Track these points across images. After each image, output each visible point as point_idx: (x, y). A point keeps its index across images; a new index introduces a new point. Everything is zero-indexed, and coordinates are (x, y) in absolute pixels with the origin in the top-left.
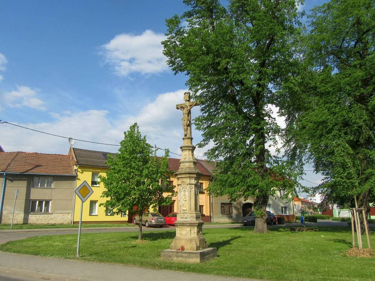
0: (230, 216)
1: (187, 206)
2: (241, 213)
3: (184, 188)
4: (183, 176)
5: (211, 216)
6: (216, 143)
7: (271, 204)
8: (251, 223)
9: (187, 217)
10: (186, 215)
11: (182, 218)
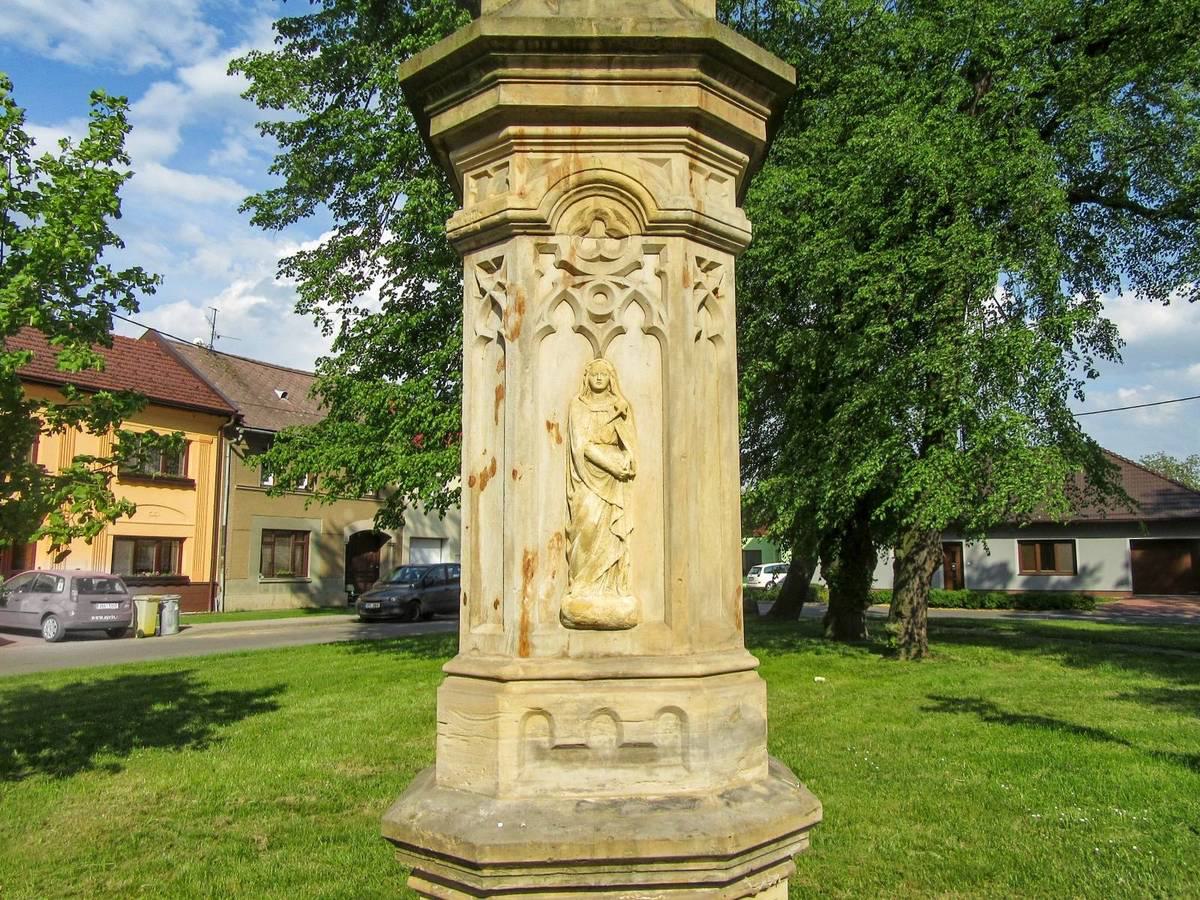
0: (300, 586)
1: (644, 554)
2: (341, 568)
3: (601, 274)
4: (592, 96)
5: (214, 585)
6: (343, 222)
7: (447, 539)
8: (396, 611)
9: (663, 732)
10: (638, 705)
11: (571, 752)
